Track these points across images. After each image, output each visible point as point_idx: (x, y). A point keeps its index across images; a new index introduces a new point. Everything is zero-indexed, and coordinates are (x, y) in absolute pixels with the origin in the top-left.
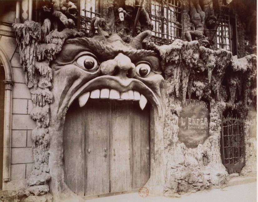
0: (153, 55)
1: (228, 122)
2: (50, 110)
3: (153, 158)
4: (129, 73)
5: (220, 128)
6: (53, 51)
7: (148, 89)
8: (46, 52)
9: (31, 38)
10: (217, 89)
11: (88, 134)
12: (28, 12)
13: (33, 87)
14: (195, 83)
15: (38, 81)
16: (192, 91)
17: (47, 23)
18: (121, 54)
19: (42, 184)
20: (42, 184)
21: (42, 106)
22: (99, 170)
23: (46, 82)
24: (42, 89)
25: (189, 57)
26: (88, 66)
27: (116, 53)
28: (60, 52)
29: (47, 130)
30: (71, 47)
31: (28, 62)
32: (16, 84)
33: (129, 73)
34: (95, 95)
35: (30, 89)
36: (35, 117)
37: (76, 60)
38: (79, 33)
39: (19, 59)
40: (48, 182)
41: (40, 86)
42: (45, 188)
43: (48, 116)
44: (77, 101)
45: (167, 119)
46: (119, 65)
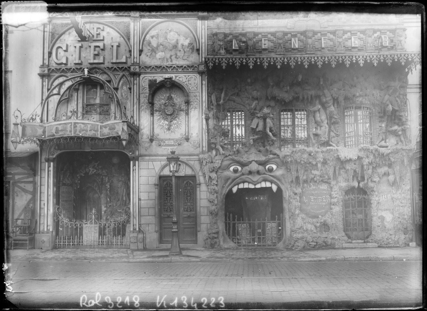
0: (276, 158)
1: (350, 199)
2: (217, 196)
3: (48, 249)
4: (258, 173)
5: (341, 203)
6: (216, 167)
7: (274, 180)
8: (214, 168)
9: (207, 162)
10: (330, 175)
11: (17, 299)
12: (205, 147)
13: (209, 185)
14: (313, 172)
15: (211, 182)
16: (311, 178)
17: (214, 152)
18: (253, 162)
19: (214, 233)
20: (214, 233)
21: (213, 195)
22: (399, 218)
23: (214, 182)
24: (213, 186)
25: (299, 158)
26: (236, 171)
27: (251, 162)
28: (220, 167)
29: (216, 206)
30: (226, 163)
31: (206, 173)
32: (201, 184)
33: (258, 173)
34: (241, 186)
35: (207, 186)
36: (210, 200)
37: (229, 168)
38: (231, 154)
39: (202, 172)
40: (217, 233)
41: (212, 184)
42: (216, 236)
43: (216, 199)
44: (231, 190)
45: (290, 198)
46: (251, 170)
